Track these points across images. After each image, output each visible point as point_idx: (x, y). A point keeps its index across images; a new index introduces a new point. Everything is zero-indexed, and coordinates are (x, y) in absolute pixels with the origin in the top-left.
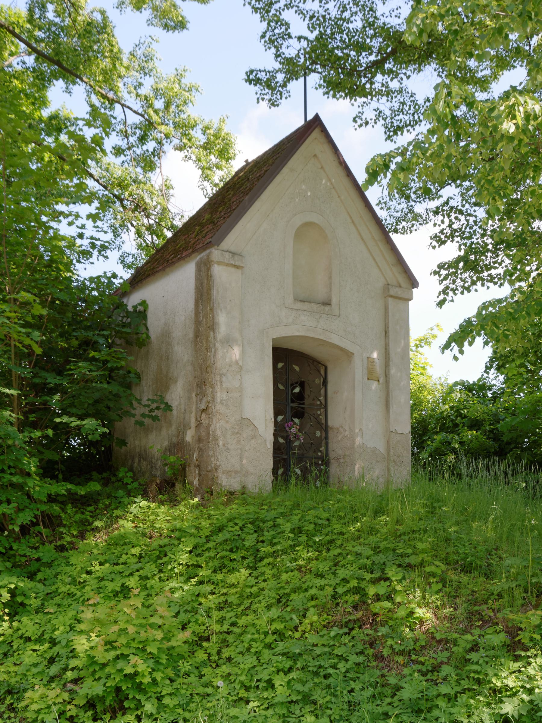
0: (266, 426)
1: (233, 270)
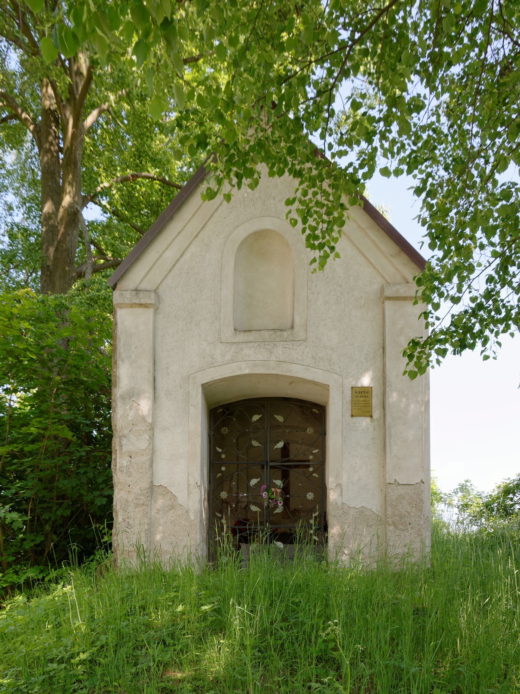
0: (189, 493)
1: (140, 310)
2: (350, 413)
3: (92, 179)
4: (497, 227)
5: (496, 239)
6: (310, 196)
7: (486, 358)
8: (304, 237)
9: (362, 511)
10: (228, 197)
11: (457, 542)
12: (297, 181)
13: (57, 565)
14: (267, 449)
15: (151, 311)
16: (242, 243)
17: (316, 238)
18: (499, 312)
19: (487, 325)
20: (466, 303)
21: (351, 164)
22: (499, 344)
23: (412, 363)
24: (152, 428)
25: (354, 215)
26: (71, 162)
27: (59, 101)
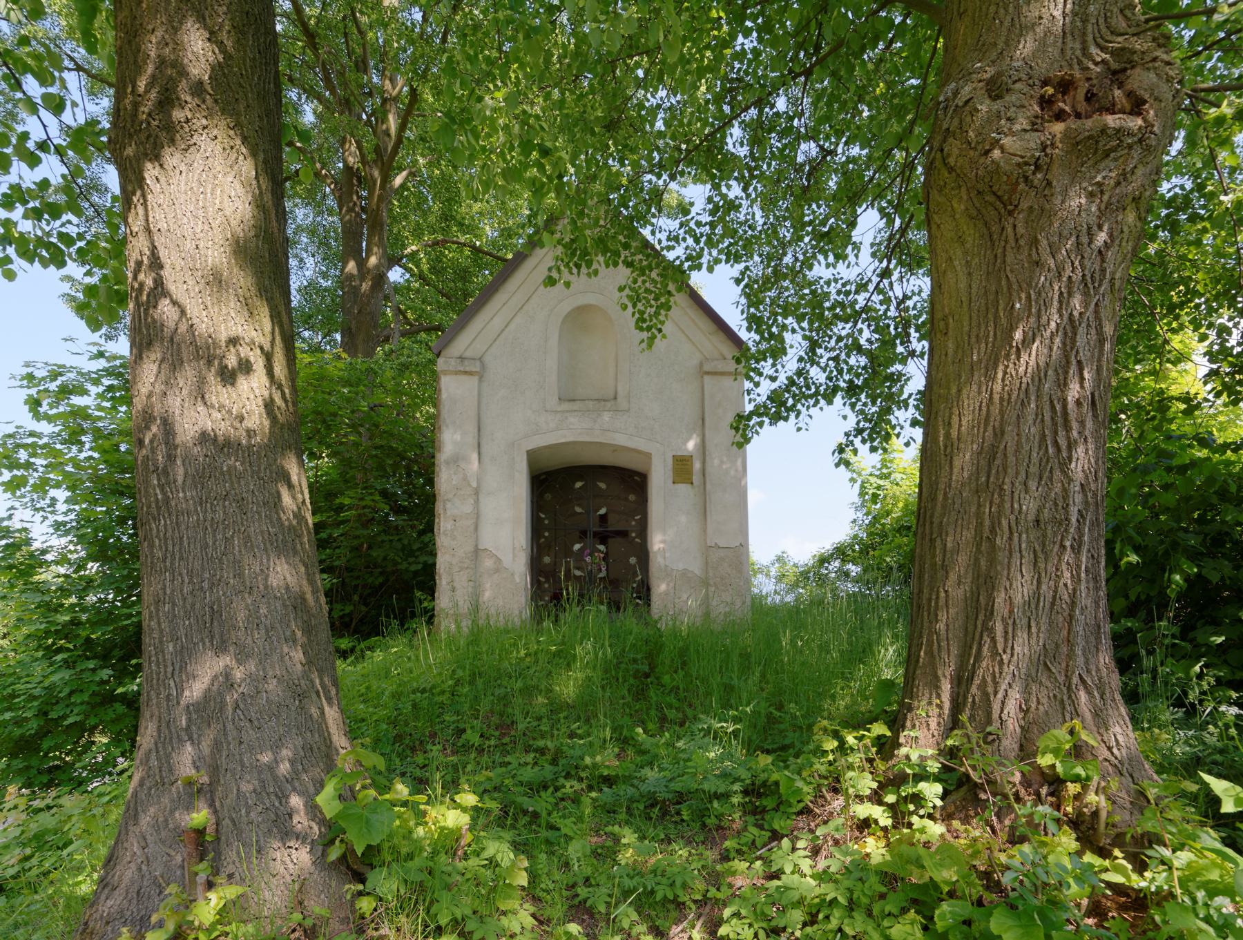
0: (514, 556)
2: (671, 480)
3: (401, 243)
4: (807, 314)
5: (805, 325)
6: (639, 283)
7: (799, 429)
8: (634, 319)
9: (685, 573)
10: (568, 285)
11: (775, 609)
12: (630, 270)
13: (367, 636)
14: (588, 513)
15: (476, 378)
16: (566, 316)
17: (644, 321)
18: (809, 388)
19: (799, 401)
20: (782, 379)
21: (678, 258)
22: (810, 417)
23: (739, 435)
24: (477, 492)
25: (680, 299)
26: (376, 225)
27: (363, 160)
